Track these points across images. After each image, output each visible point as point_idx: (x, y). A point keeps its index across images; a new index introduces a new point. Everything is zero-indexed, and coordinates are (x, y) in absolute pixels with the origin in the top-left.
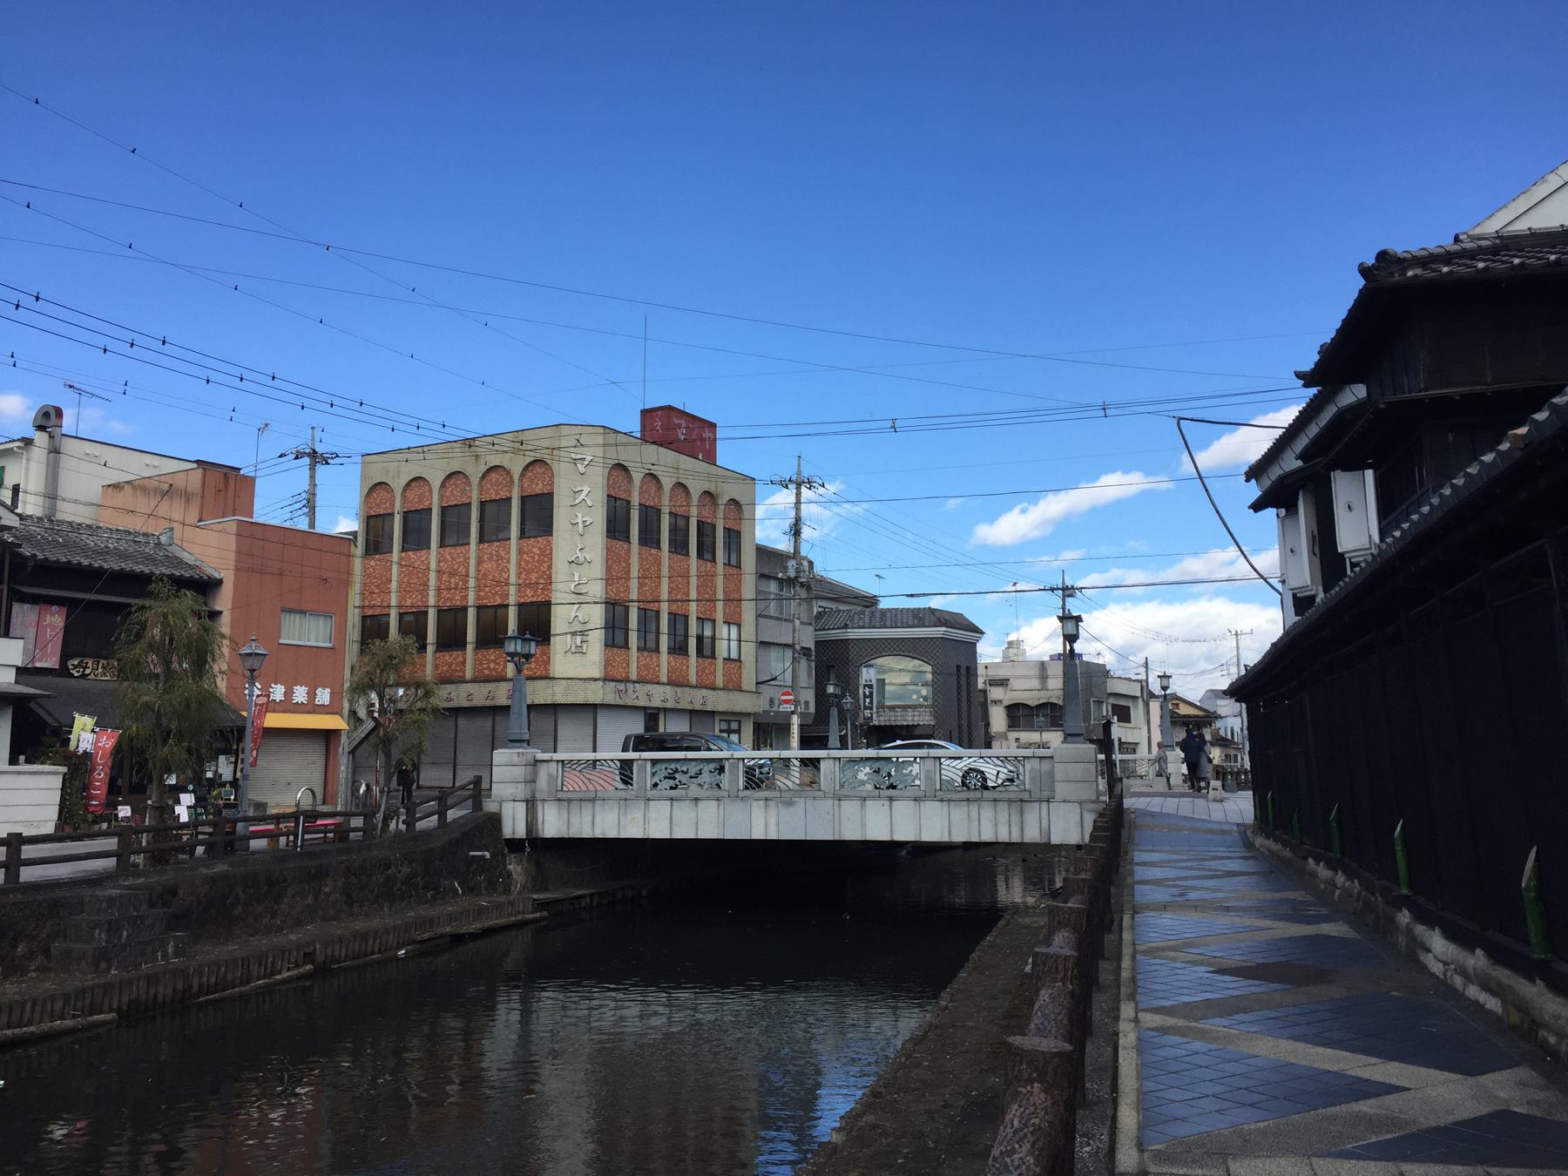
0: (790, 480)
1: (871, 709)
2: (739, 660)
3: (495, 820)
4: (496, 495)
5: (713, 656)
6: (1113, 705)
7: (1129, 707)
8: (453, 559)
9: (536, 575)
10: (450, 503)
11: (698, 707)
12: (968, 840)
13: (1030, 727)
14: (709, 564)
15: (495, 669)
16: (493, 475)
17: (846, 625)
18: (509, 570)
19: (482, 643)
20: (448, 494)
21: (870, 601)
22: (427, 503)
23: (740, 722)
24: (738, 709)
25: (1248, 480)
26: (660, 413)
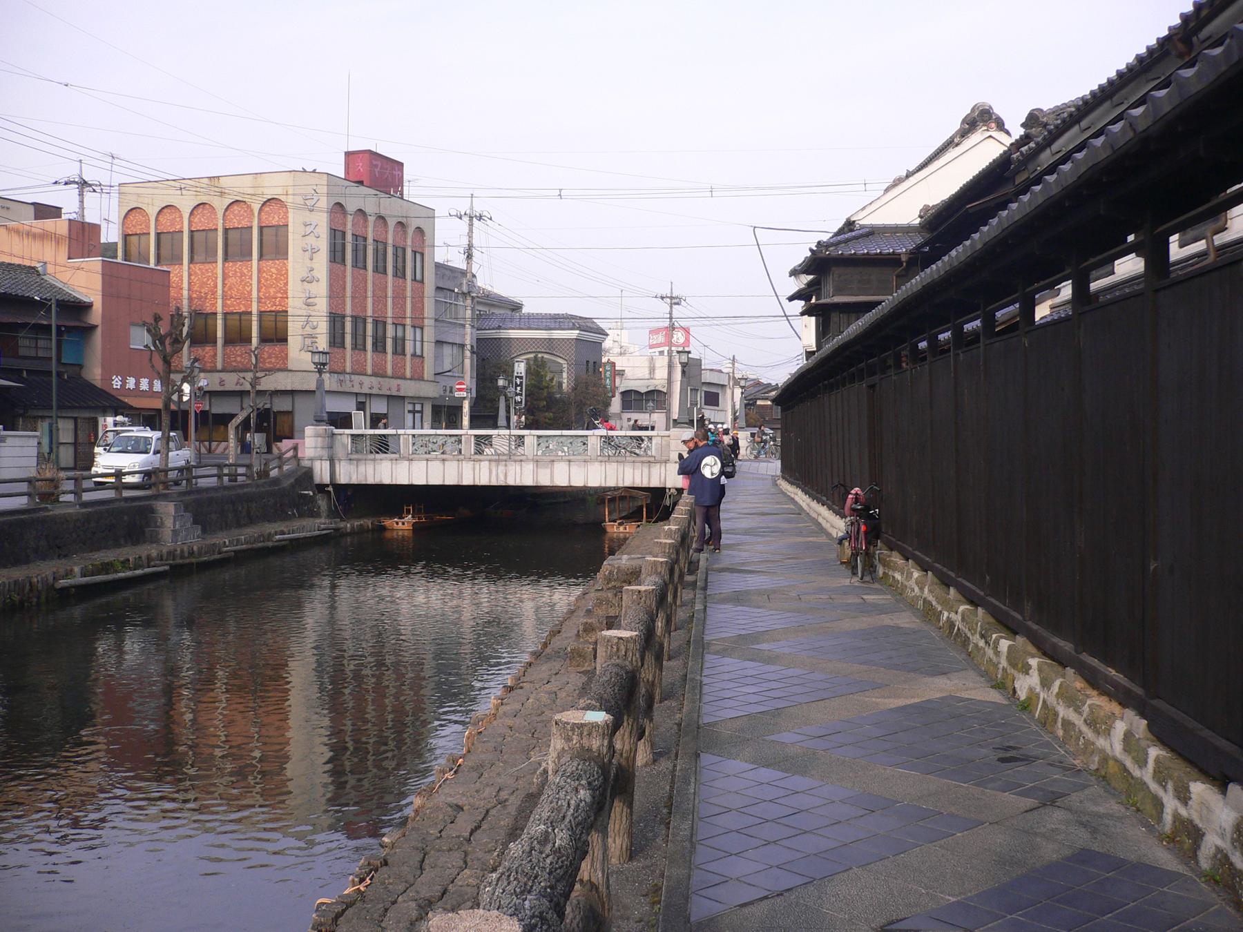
0: (465, 214)
1: (521, 395)
2: (422, 356)
3: (309, 473)
4: (239, 224)
5: (403, 353)
6: (705, 392)
7: (718, 394)
8: (203, 274)
9: (274, 290)
10: (198, 228)
11: (394, 393)
13: (640, 409)
14: (401, 280)
15: (240, 362)
16: (235, 207)
17: (499, 326)
18: (251, 284)
19: (228, 341)
20: (196, 220)
21: (516, 307)
22: (178, 227)
23: (422, 404)
24: (422, 394)
25: (790, 276)
26: (361, 155)
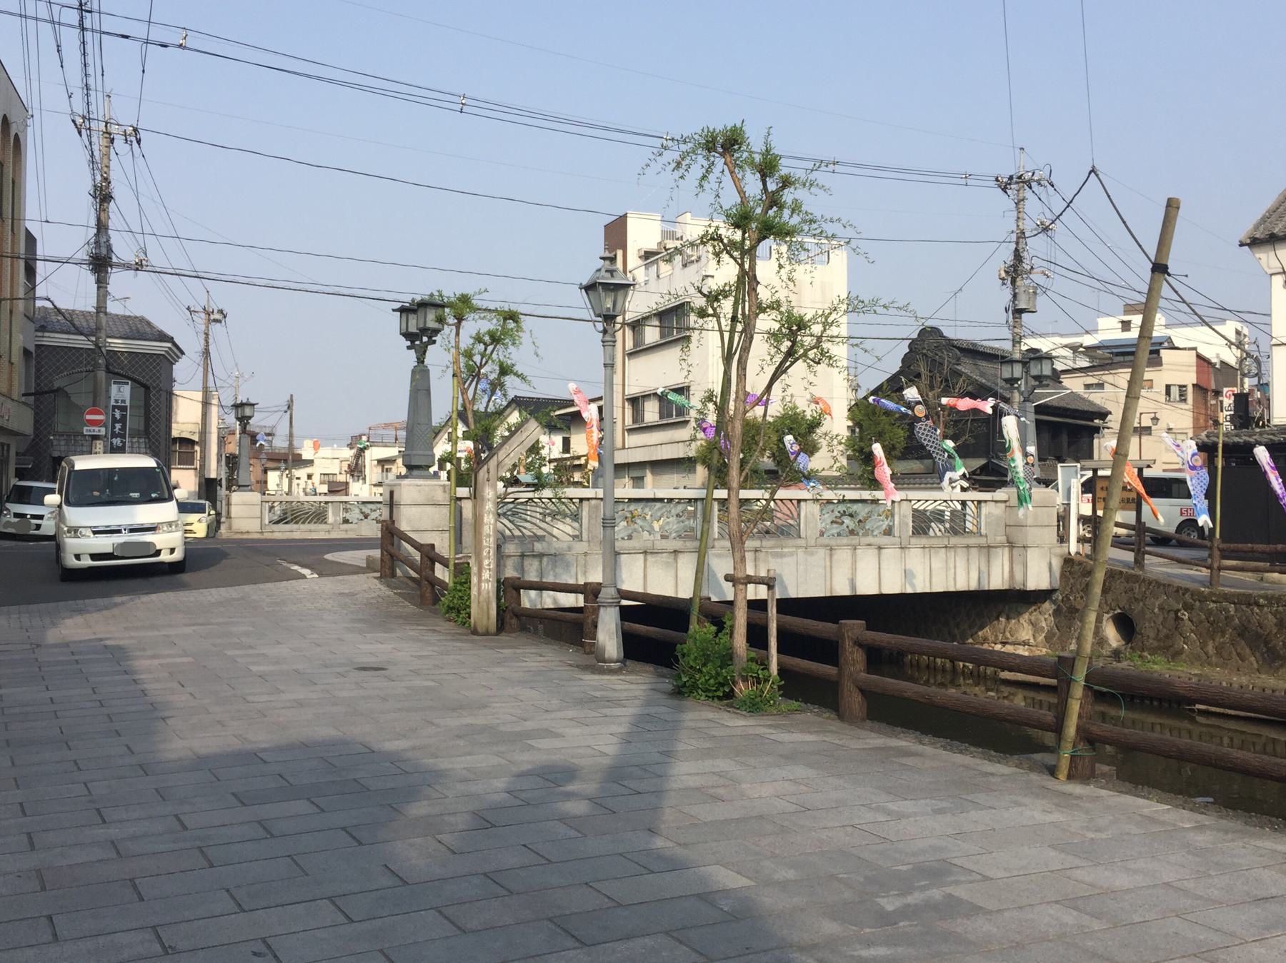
1: (123, 436)
12: (946, 590)
